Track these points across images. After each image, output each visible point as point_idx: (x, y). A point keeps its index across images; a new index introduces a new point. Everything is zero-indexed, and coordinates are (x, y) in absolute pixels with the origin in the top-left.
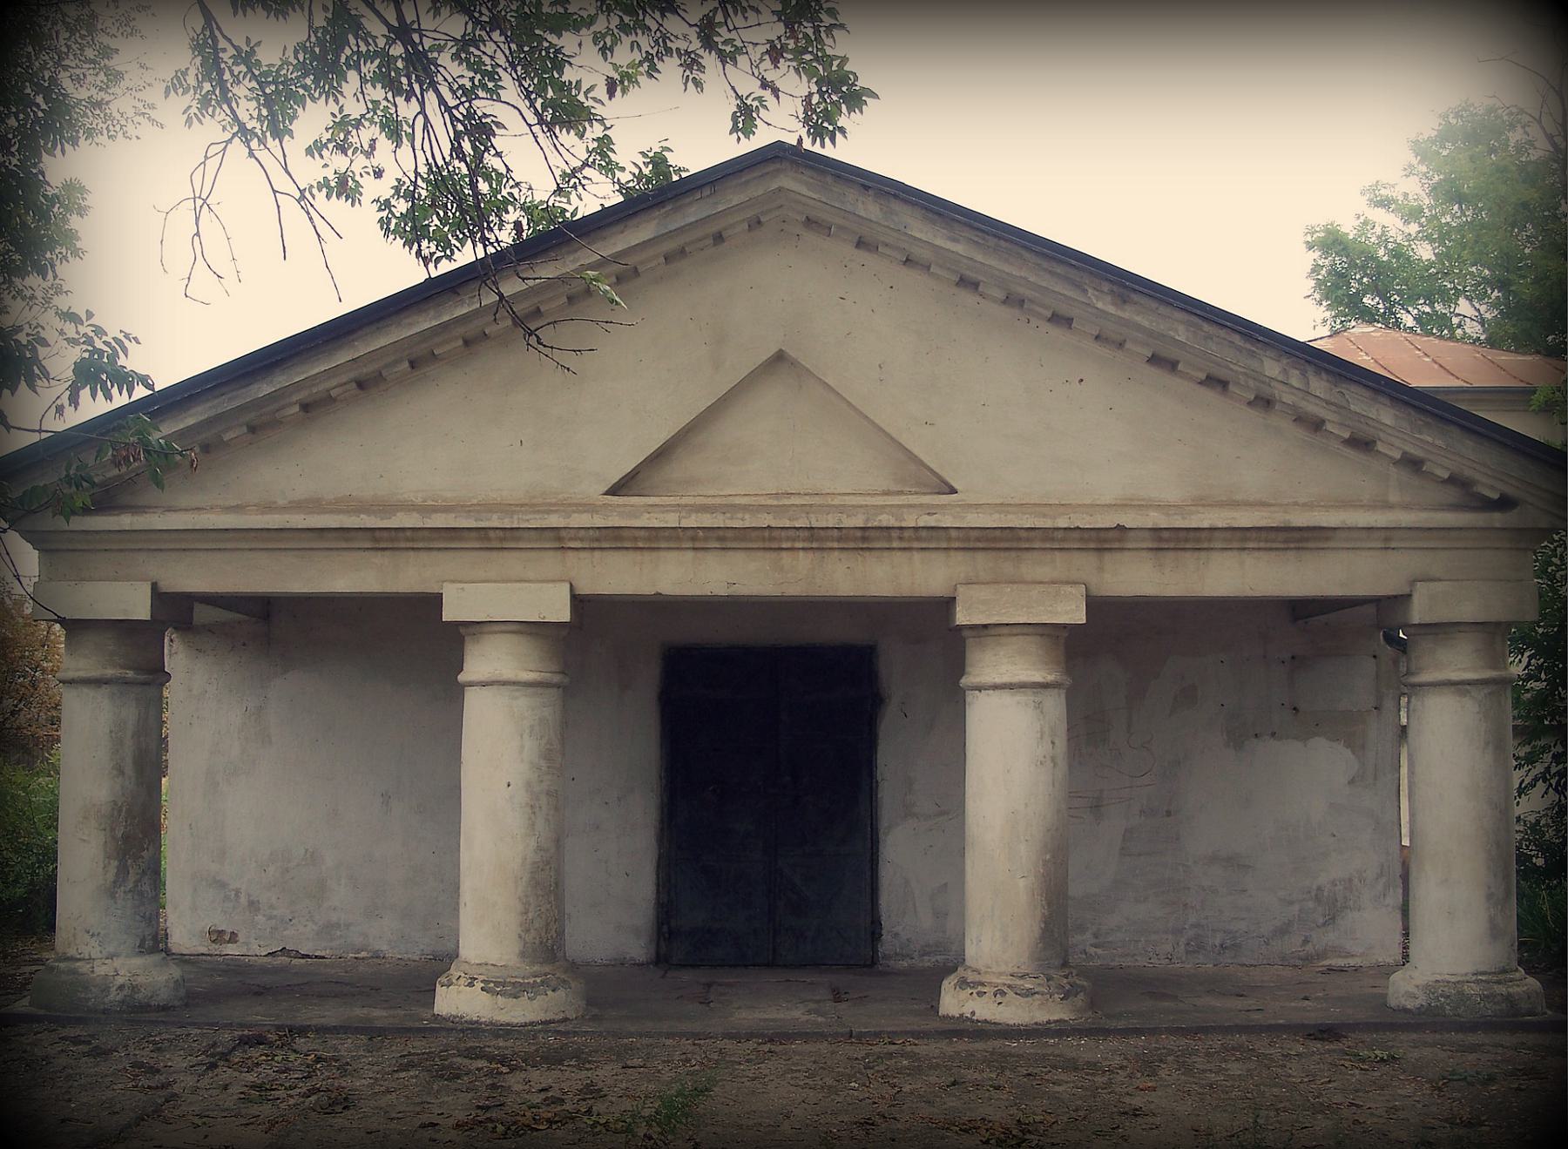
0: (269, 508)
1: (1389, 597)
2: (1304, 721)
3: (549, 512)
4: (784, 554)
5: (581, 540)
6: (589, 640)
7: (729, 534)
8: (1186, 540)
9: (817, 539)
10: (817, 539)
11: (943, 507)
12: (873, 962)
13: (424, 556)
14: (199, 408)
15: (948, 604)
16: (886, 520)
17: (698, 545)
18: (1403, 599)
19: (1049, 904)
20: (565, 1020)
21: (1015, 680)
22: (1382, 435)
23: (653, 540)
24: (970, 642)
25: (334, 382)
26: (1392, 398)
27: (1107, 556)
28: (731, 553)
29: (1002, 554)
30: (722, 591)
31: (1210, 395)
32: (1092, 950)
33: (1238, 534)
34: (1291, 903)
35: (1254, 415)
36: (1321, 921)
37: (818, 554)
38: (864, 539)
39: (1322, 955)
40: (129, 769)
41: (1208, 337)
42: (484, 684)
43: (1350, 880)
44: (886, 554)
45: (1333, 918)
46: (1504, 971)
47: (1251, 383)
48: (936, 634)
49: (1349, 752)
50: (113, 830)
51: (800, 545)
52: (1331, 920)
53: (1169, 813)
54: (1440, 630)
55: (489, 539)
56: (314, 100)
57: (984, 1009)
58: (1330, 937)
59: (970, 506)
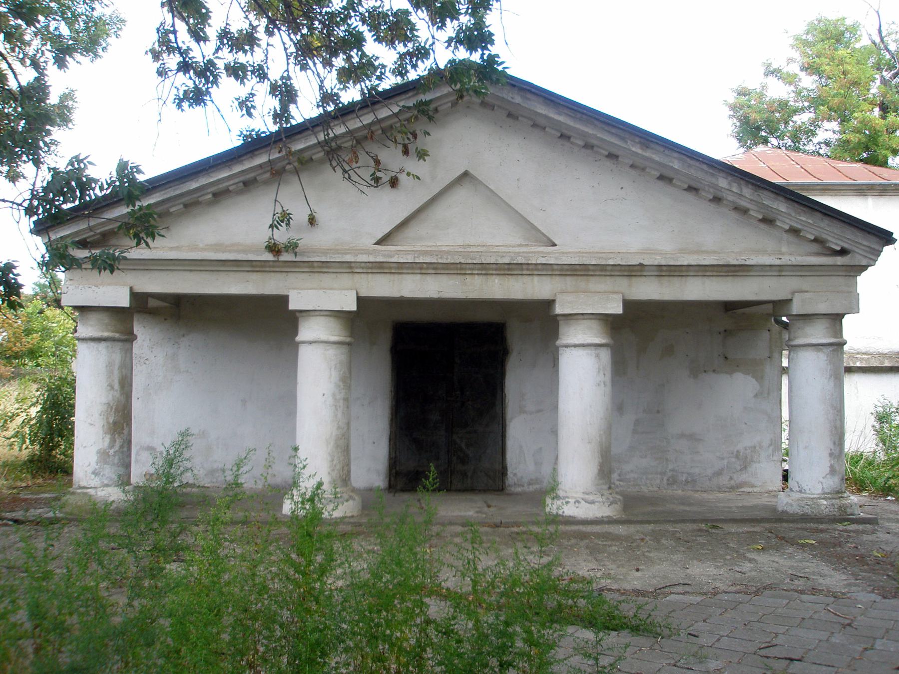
0: (195, 248)
1: (780, 301)
2: (729, 363)
3: (346, 254)
4: (468, 277)
5: (363, 268)
6: (367, 321)
7: (440, 266)
8: (675, 271)
9: (485, 269)
10: (485, 269)
11: (549, 253)
12: (503, 489)
13: (278, 275)
14: (157, 194)
15: (550, 303)
16: (520, 260)
17: (423, 271)
18: (789, 301)
19: (602, 456)
20: (352, 517)
21: (586, 342)
22: (779, 217)
23: (401, 268)
24: (561, 323)
25: (232, 182)
26: (786, 198)
27: (634, 279)
28: (440, 276)
29: (580, 278)
30: (435, 296)
31: (690, 196)
32: (617, 483)
33: (703, 268)
34: (723, 459)
35: (713, 206)
36: (739, 468)
37: (484, 277)
38: (509, 269)
39: (739, 486)
40: (117, 386)
41: (690, 166)
42: (311, 343)
43: (755, 447)
44: (520, 277)
45: (745, 467)
46: (838, 492)
47: (711, 190)
48: (542, 320)
49: (754, 380)
50: (107, 418)
51: (476, 272)
52: (745, 468)
53: (658, 412)
54: (807, 318)
55: (314, 267)
56: (120, 29)
57: (569, 511)
58: (744, 477)
59: (563, 253)
